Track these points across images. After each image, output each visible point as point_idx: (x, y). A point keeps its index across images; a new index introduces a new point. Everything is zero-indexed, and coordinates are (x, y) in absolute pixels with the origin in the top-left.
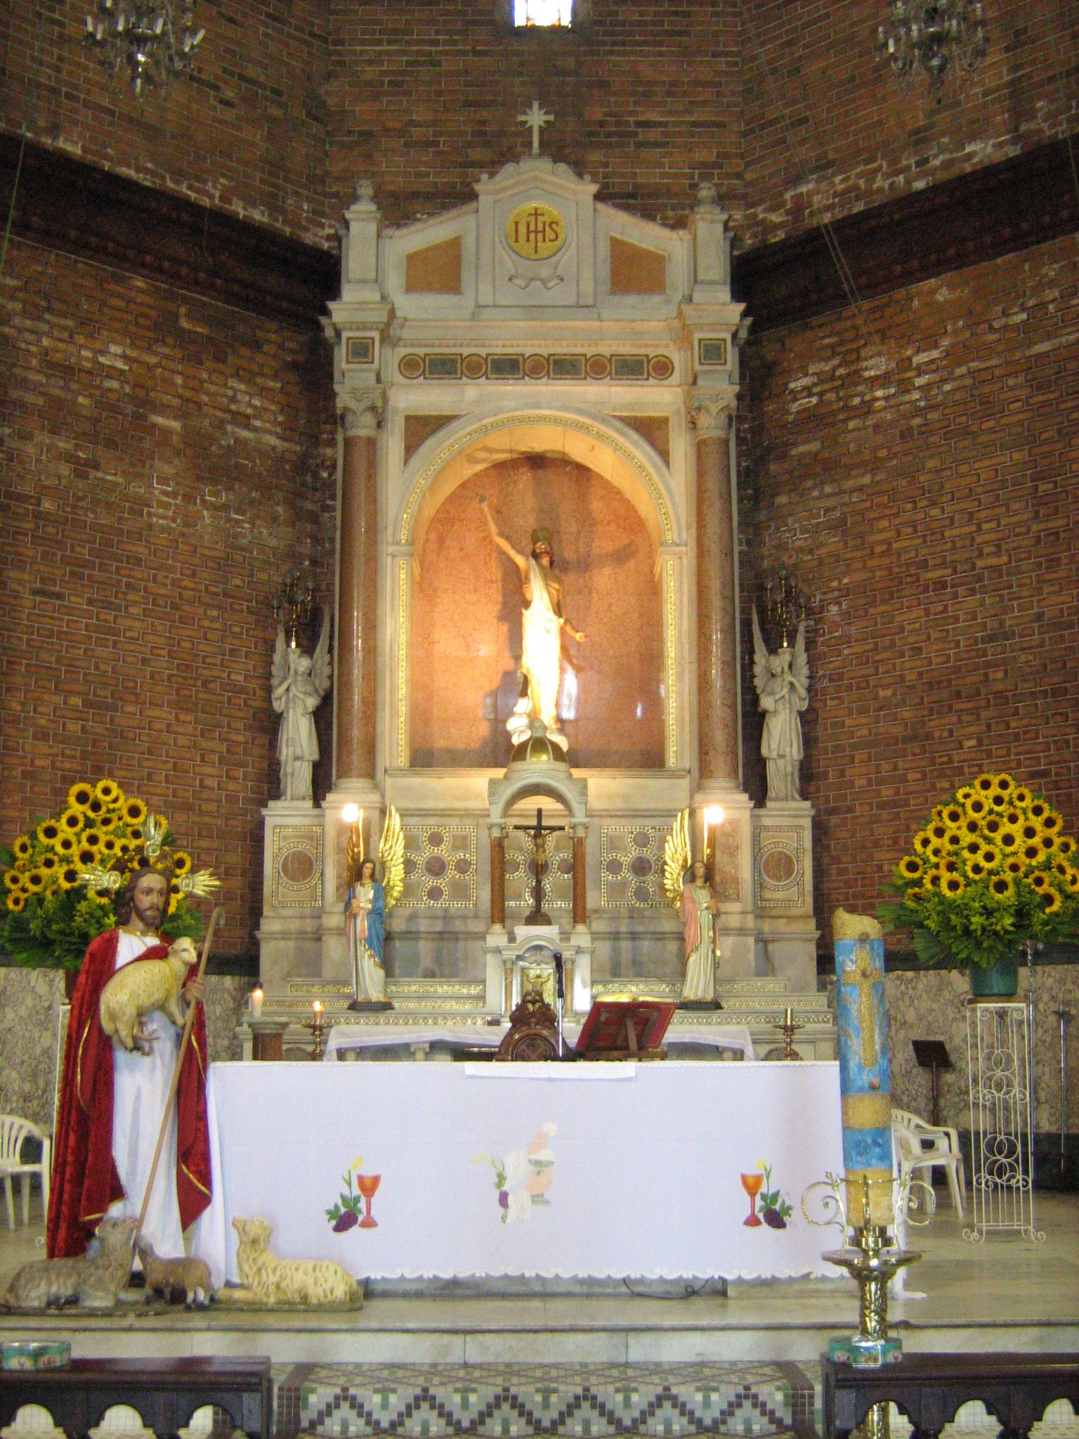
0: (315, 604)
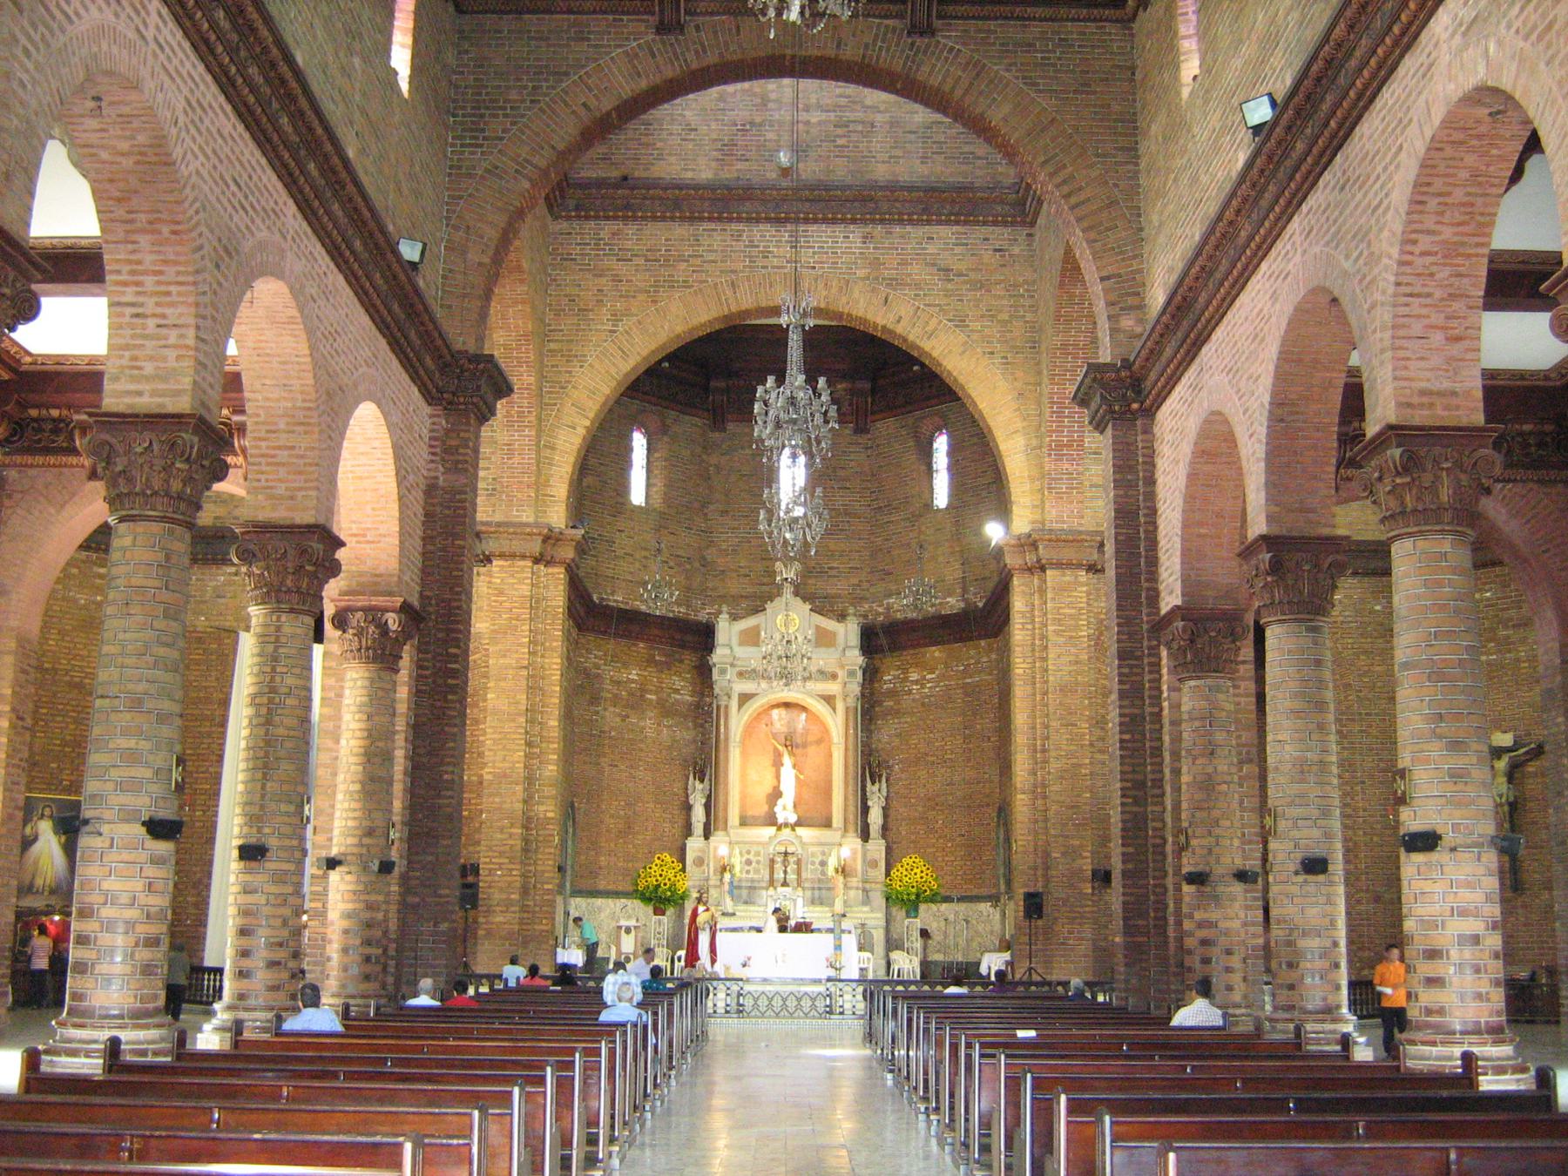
0: (704, 762)
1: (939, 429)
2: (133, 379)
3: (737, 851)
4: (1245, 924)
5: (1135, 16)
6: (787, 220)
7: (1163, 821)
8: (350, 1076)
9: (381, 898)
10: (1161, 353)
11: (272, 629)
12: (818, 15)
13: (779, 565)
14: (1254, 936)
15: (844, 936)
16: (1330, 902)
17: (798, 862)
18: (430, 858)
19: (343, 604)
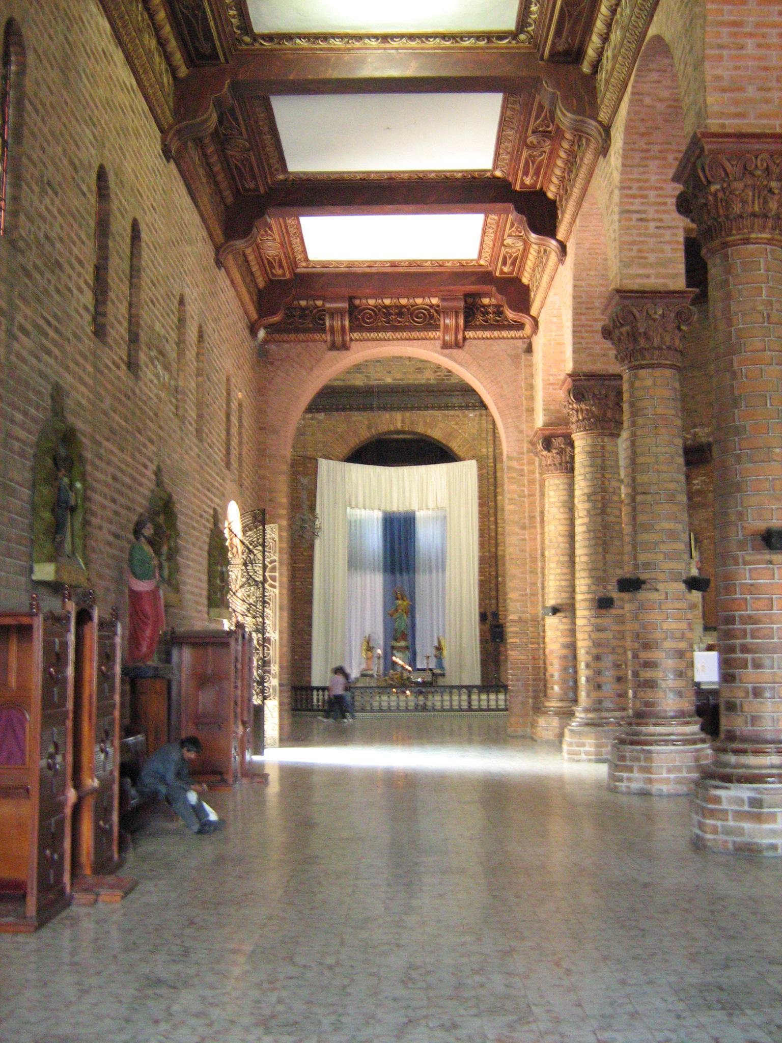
2: (643, 266)
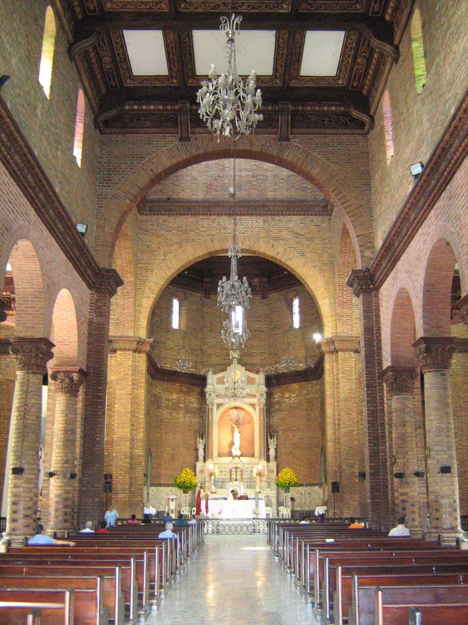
0: (203, 431)
1: (295, 296)
3: (216, 467)
4: (419, 493)
5: (369, 131)
6: (233, 215)
7: (385, 453)
8: (53, 563)
9: (71, 488)
10: (381, 265)
11: (26, 380)
12: (236, 133)
13: (231, 352)
14: (423, 498)
15: (254, 501)
16: (452, 484)
17: (241, 471)
18: (91, 472)
19: (55, 370)
